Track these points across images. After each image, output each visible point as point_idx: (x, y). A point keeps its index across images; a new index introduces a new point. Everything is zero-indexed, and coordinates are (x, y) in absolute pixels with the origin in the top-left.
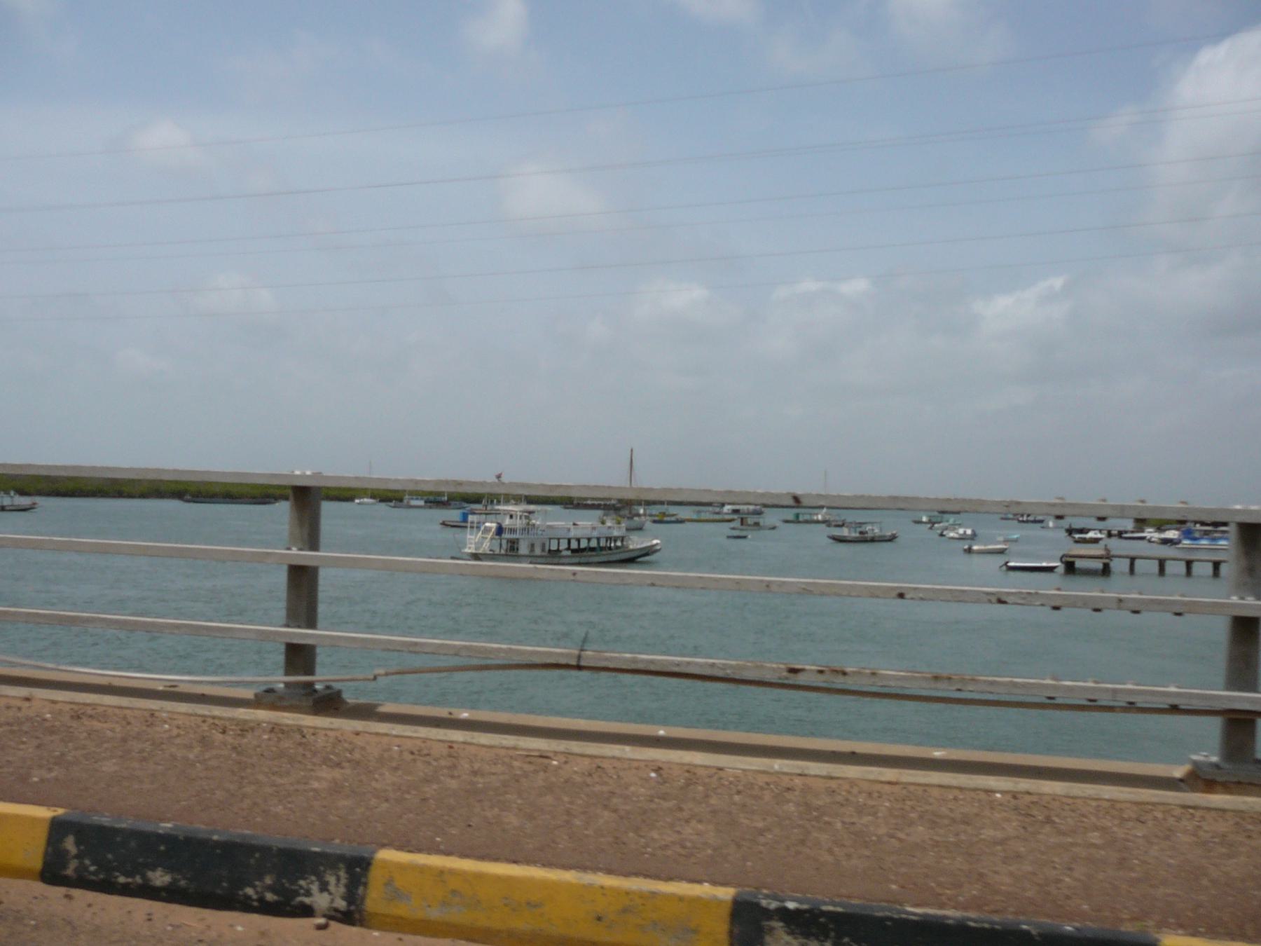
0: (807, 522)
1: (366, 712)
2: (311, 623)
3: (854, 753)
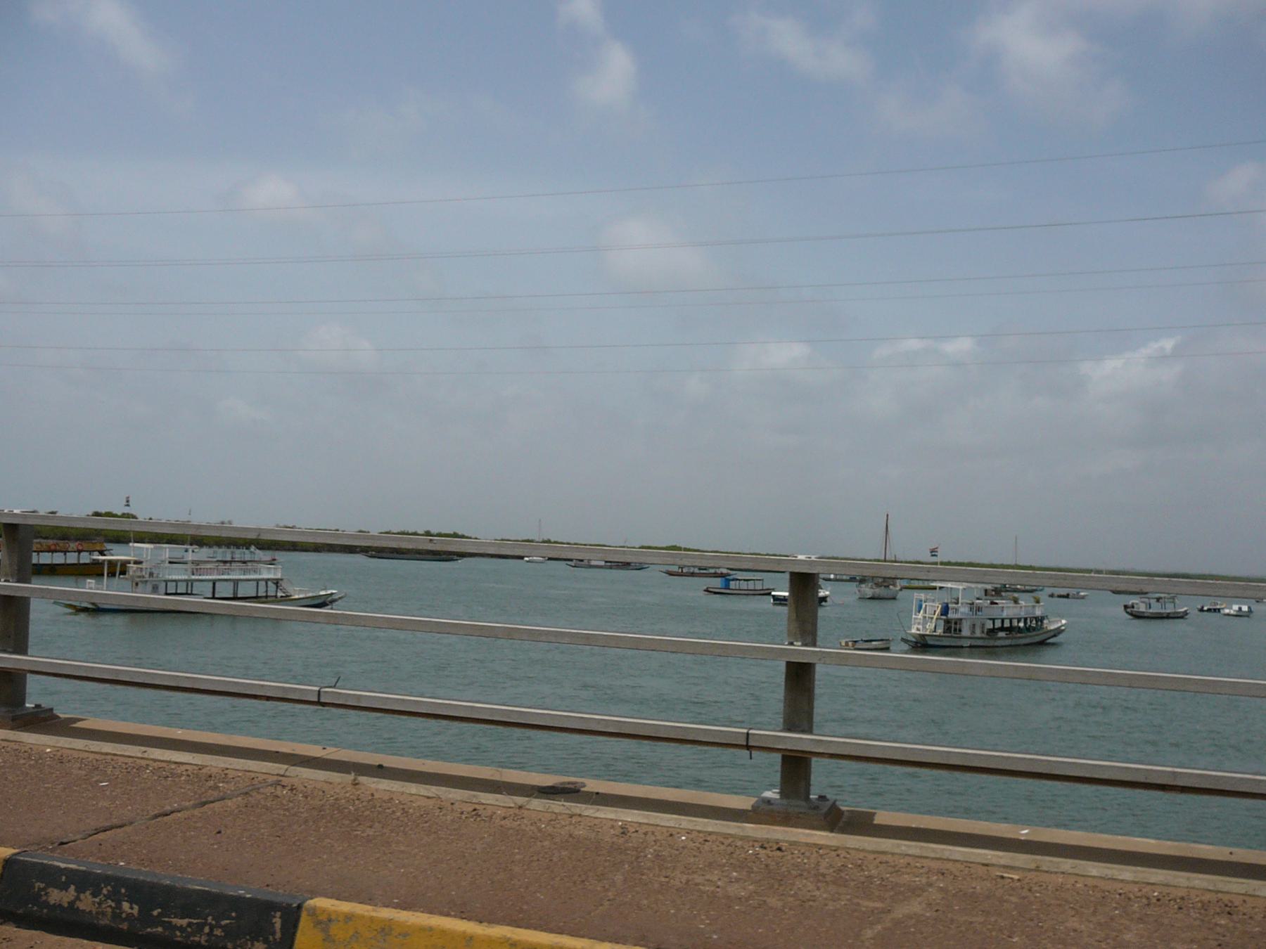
2: (21, 647)
3: (380, 766)
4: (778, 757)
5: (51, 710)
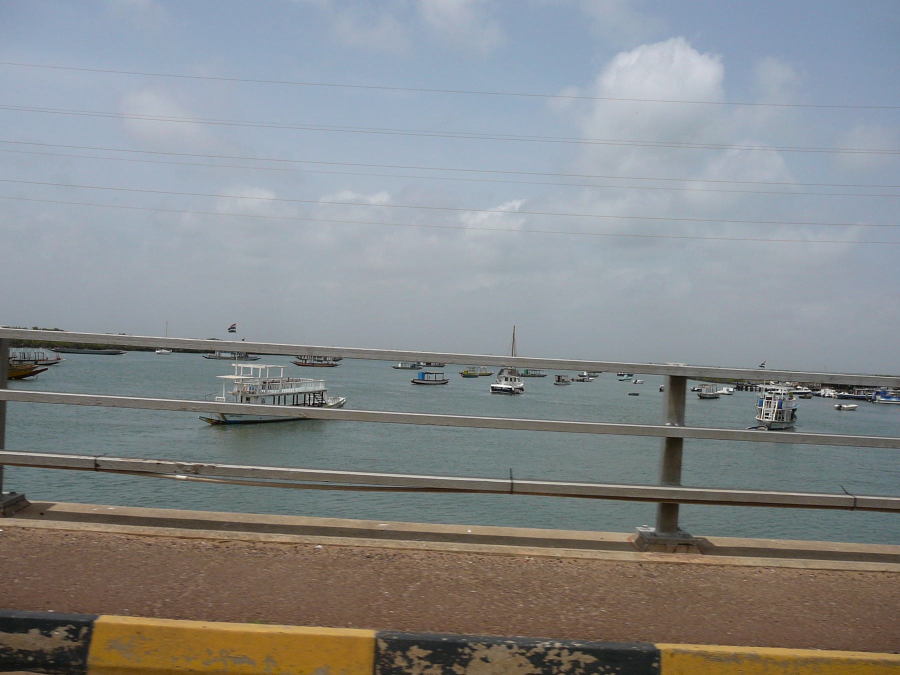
0: (534, 376)
1: (42, 512)
4: (655, 505)
5: (23, 497)
